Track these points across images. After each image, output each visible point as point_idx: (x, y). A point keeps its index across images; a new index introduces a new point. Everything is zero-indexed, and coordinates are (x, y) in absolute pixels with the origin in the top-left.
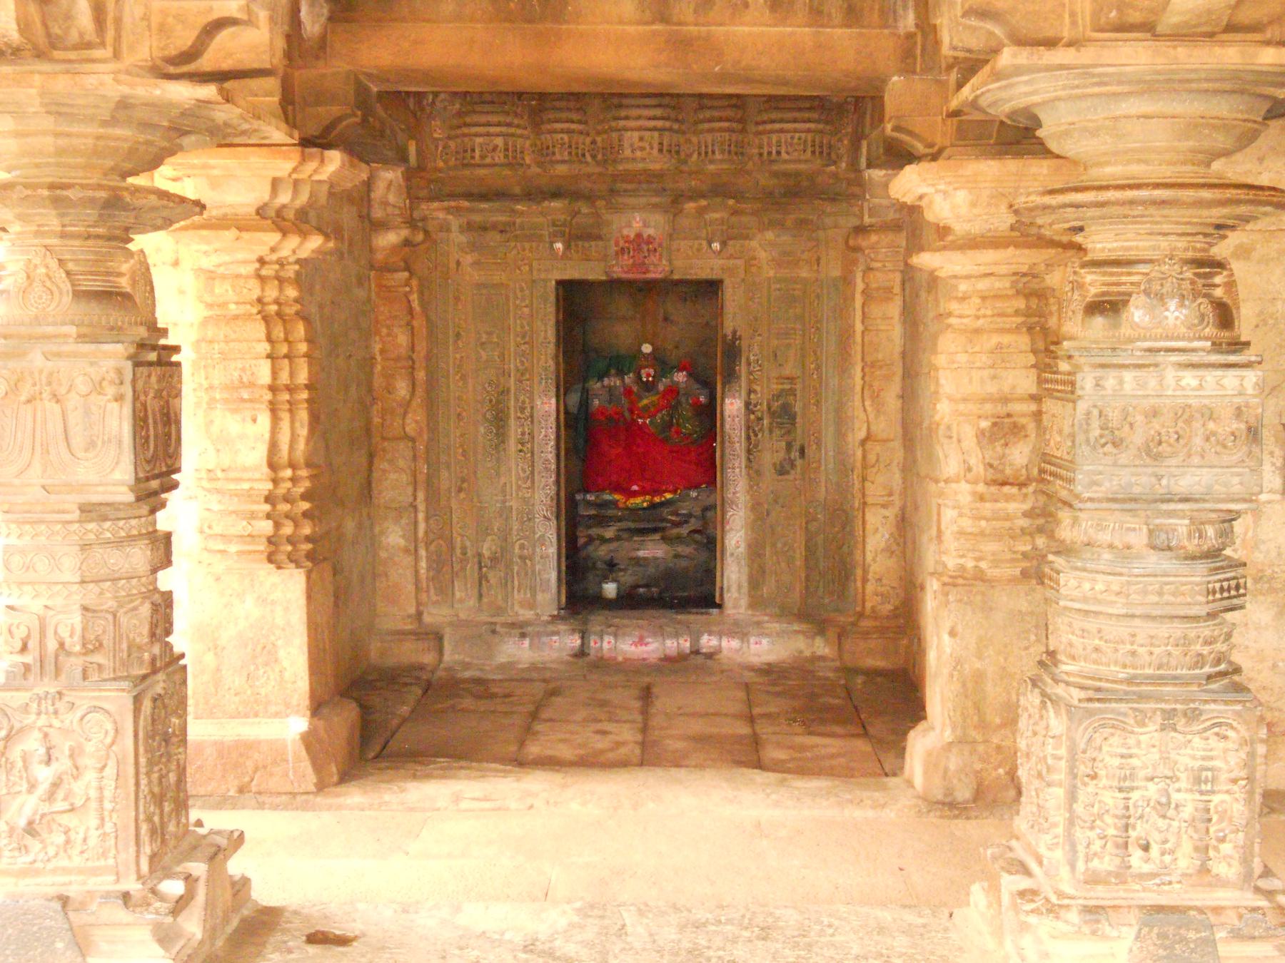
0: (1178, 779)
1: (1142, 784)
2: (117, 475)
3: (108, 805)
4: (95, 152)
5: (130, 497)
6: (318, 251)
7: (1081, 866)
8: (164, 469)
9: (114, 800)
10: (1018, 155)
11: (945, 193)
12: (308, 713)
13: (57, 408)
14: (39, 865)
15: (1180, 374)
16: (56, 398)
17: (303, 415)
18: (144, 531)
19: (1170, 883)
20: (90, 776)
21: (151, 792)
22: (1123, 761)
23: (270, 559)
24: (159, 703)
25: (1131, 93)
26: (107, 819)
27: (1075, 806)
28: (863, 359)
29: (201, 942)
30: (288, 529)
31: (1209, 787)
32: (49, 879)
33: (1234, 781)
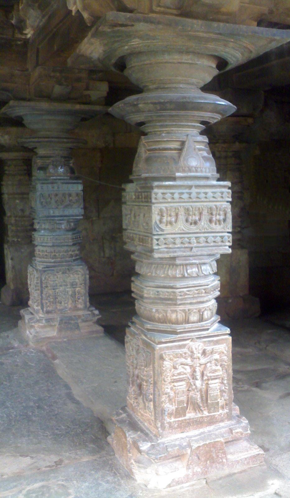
1: (58, 287)
7: (45, 309)
31: (75, 286)
33: (81, 284)
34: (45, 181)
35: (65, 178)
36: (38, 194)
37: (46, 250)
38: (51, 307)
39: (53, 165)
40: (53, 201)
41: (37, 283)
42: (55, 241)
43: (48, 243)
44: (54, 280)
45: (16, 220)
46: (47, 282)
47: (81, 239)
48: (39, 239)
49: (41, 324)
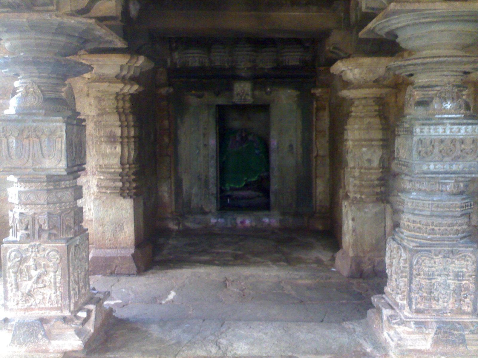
0: (450, 275)
1: (436, 277)
2: (60, 165)
3: (58, 285)
4: (50, 45)
5: (65, 173)
6: (136, 90)
7: (414, 307)
8: (79, 163)
9: (60, 283)
10: (377, 56)
11: (351, 69)
12: (134, 247)
13: (38, 140)
14: (33, 307)
15: (452, 127)
16: (38, 137)
17: (132, 146)
18: (71, 185)
19: (446, 313)
20: (52, 274)
21: (75, 280)
22: (430, 269)
23: (121, 195)
24: (77, 247)
25: (436, 22)
26: (58, 290)
27: (411, 285)
28: (316, 130)
29: (93, 334)
30: (127, 185)
31: (461, 278)
32: (37, 312)
33: (471, 276)
34: (428, 121)
35: (458, 116)
36: (416, 139)
37: (420, 221)
38: (423, 304)
39: (440, 98)
40: (436, 150)
41: (404, 267)
42: (435, 209)
43: (425, 210)
44: (430, 265)
45: (361, 173)
46: (419, 268)
47: (472, 207)
48: (409, 204)
49: (407, 329)
